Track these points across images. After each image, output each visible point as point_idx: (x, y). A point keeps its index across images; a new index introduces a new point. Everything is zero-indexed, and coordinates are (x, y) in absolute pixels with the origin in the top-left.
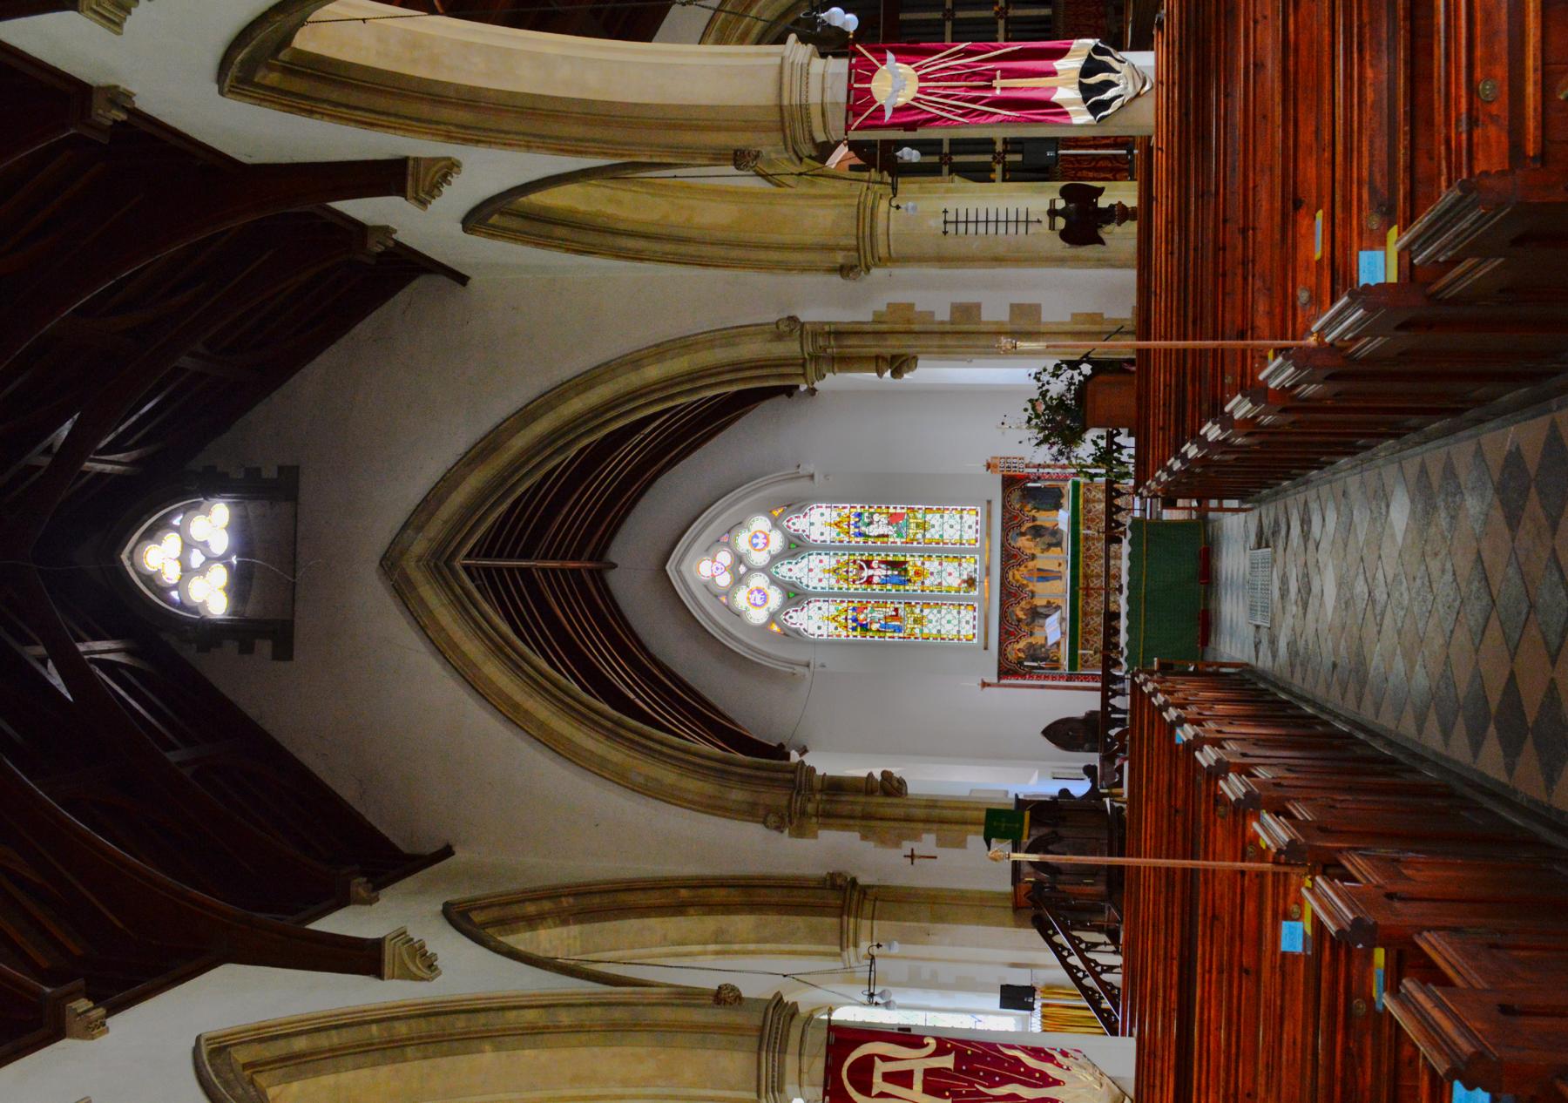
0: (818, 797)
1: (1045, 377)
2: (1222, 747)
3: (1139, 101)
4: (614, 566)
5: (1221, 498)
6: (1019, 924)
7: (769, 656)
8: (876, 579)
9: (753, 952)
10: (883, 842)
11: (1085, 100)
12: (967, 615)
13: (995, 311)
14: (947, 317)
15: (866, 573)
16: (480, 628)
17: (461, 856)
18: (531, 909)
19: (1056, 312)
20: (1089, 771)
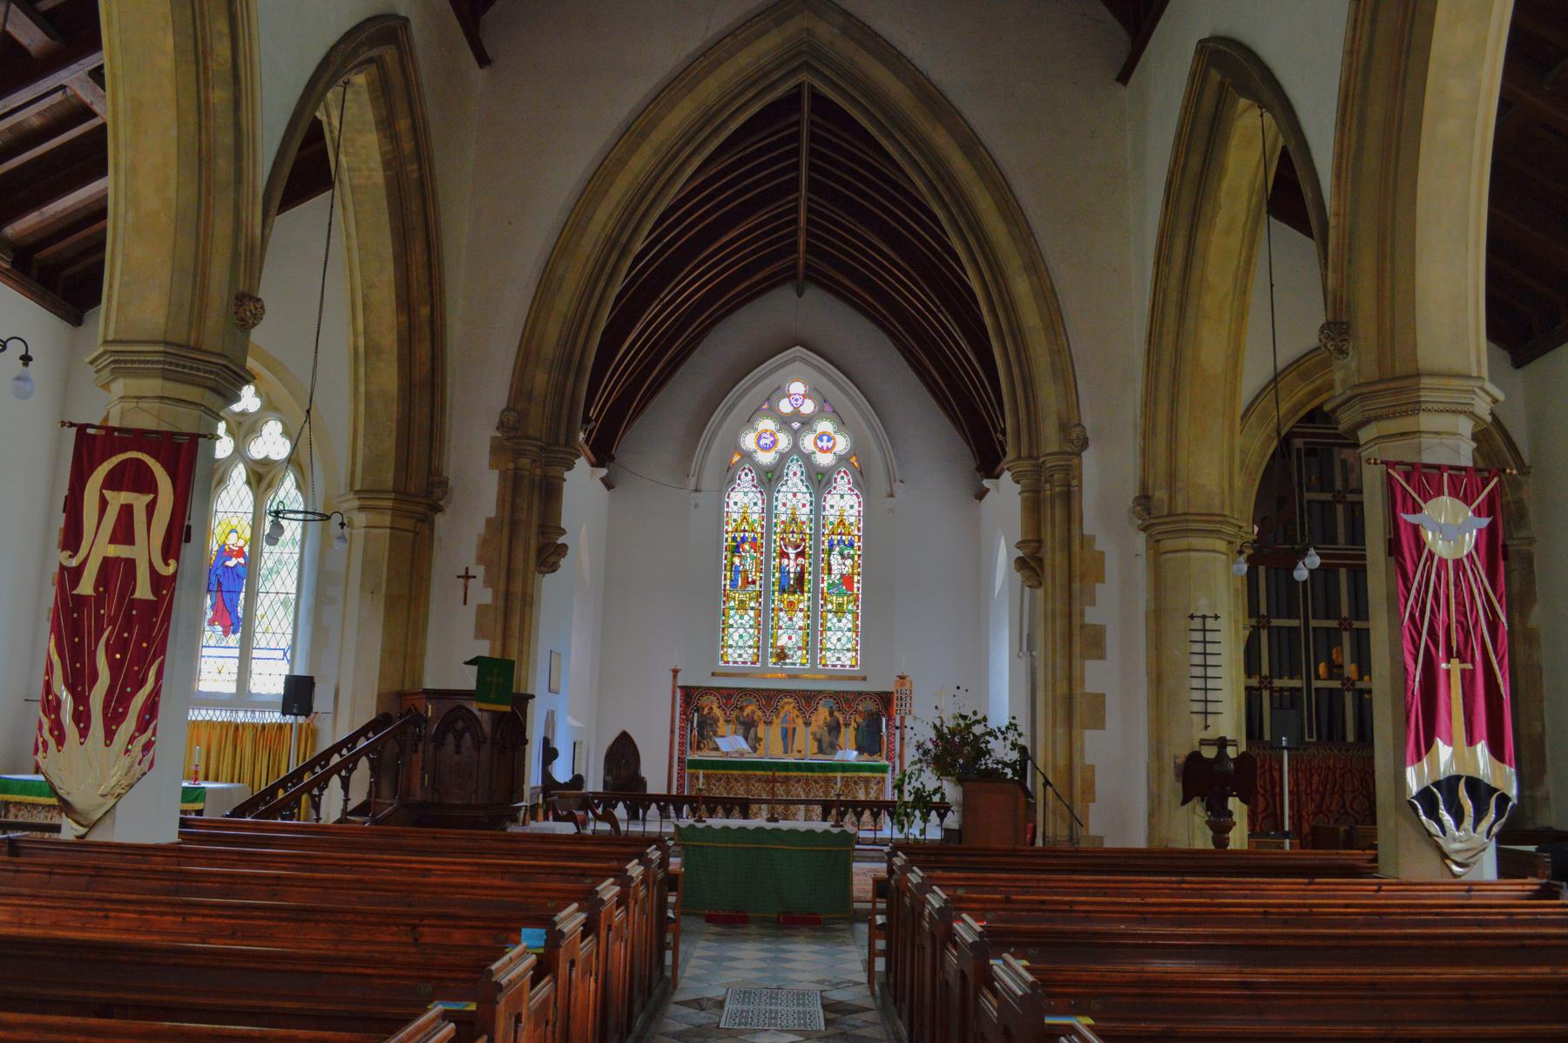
0: (538, 471)
1: (1011, 736)
2: (584, 936)
3: (1434, 858)
4: (800, 294)
5: (887, 953)
6: (382, 698)
7: (707, 449)
8: (785, 561)
9: (356, 388)
10: (484, 543)
11: (1437, 784)
12: (748, 654)
13: (1096, 676)
14: (1088, 620)
15: (792, 552)
16: (734, 98)
17: (478, 75)
18: (403, 124)
19: (1096, 747)
20: (577, 781)
